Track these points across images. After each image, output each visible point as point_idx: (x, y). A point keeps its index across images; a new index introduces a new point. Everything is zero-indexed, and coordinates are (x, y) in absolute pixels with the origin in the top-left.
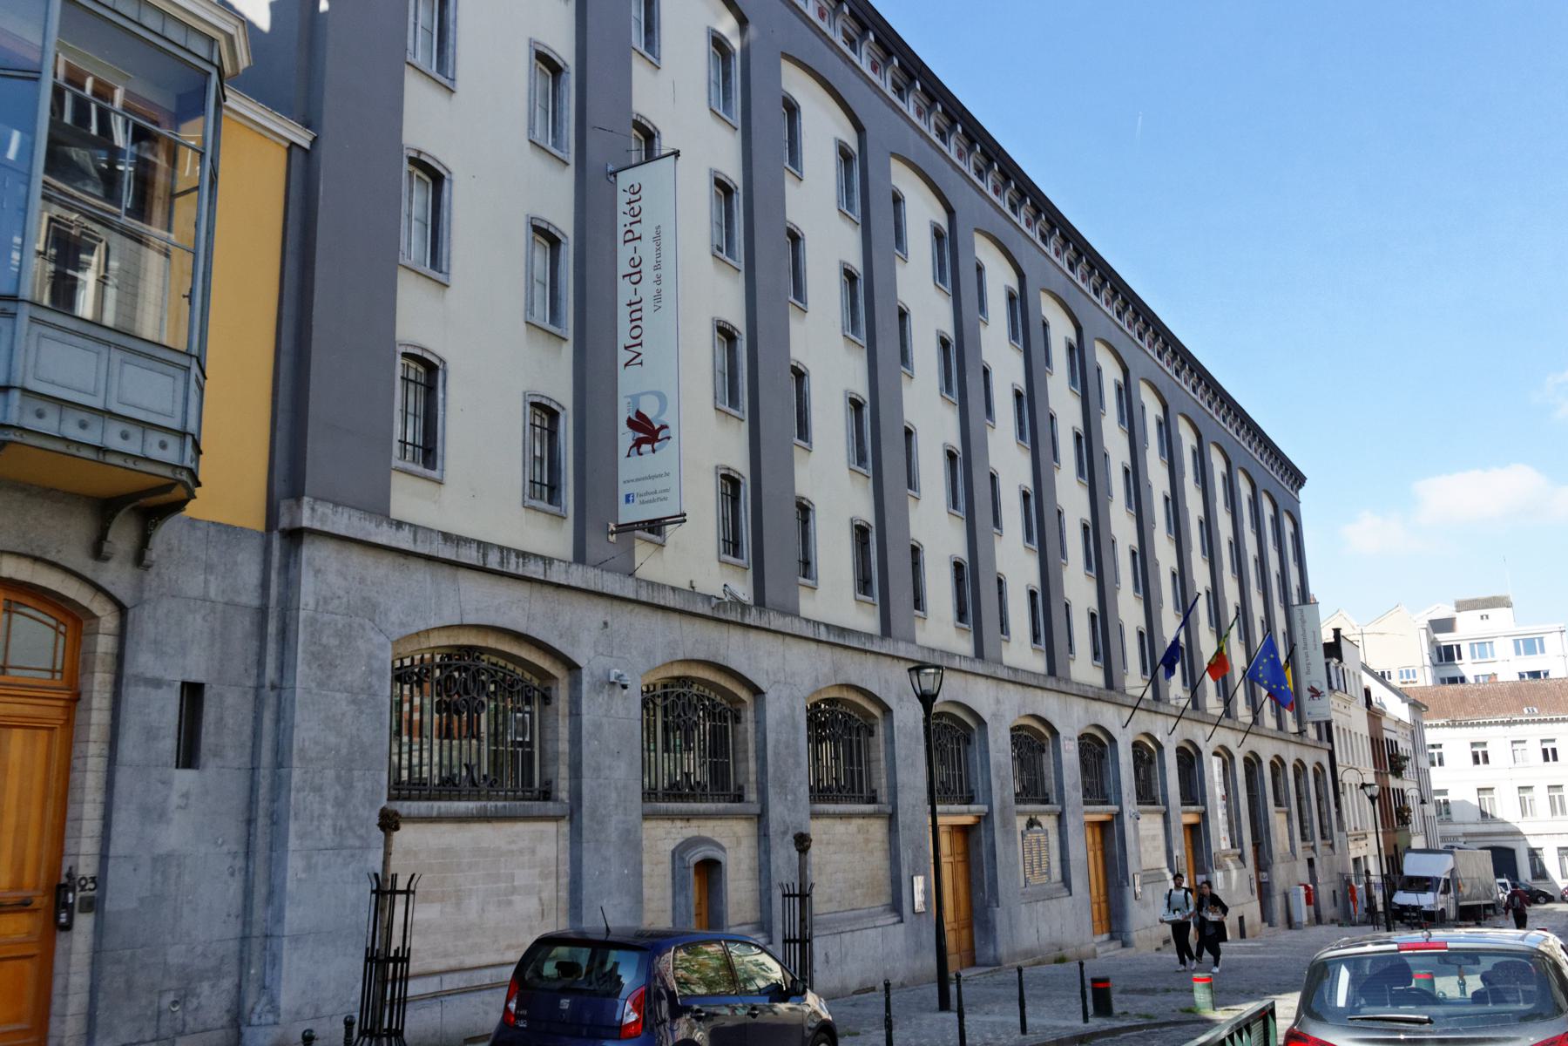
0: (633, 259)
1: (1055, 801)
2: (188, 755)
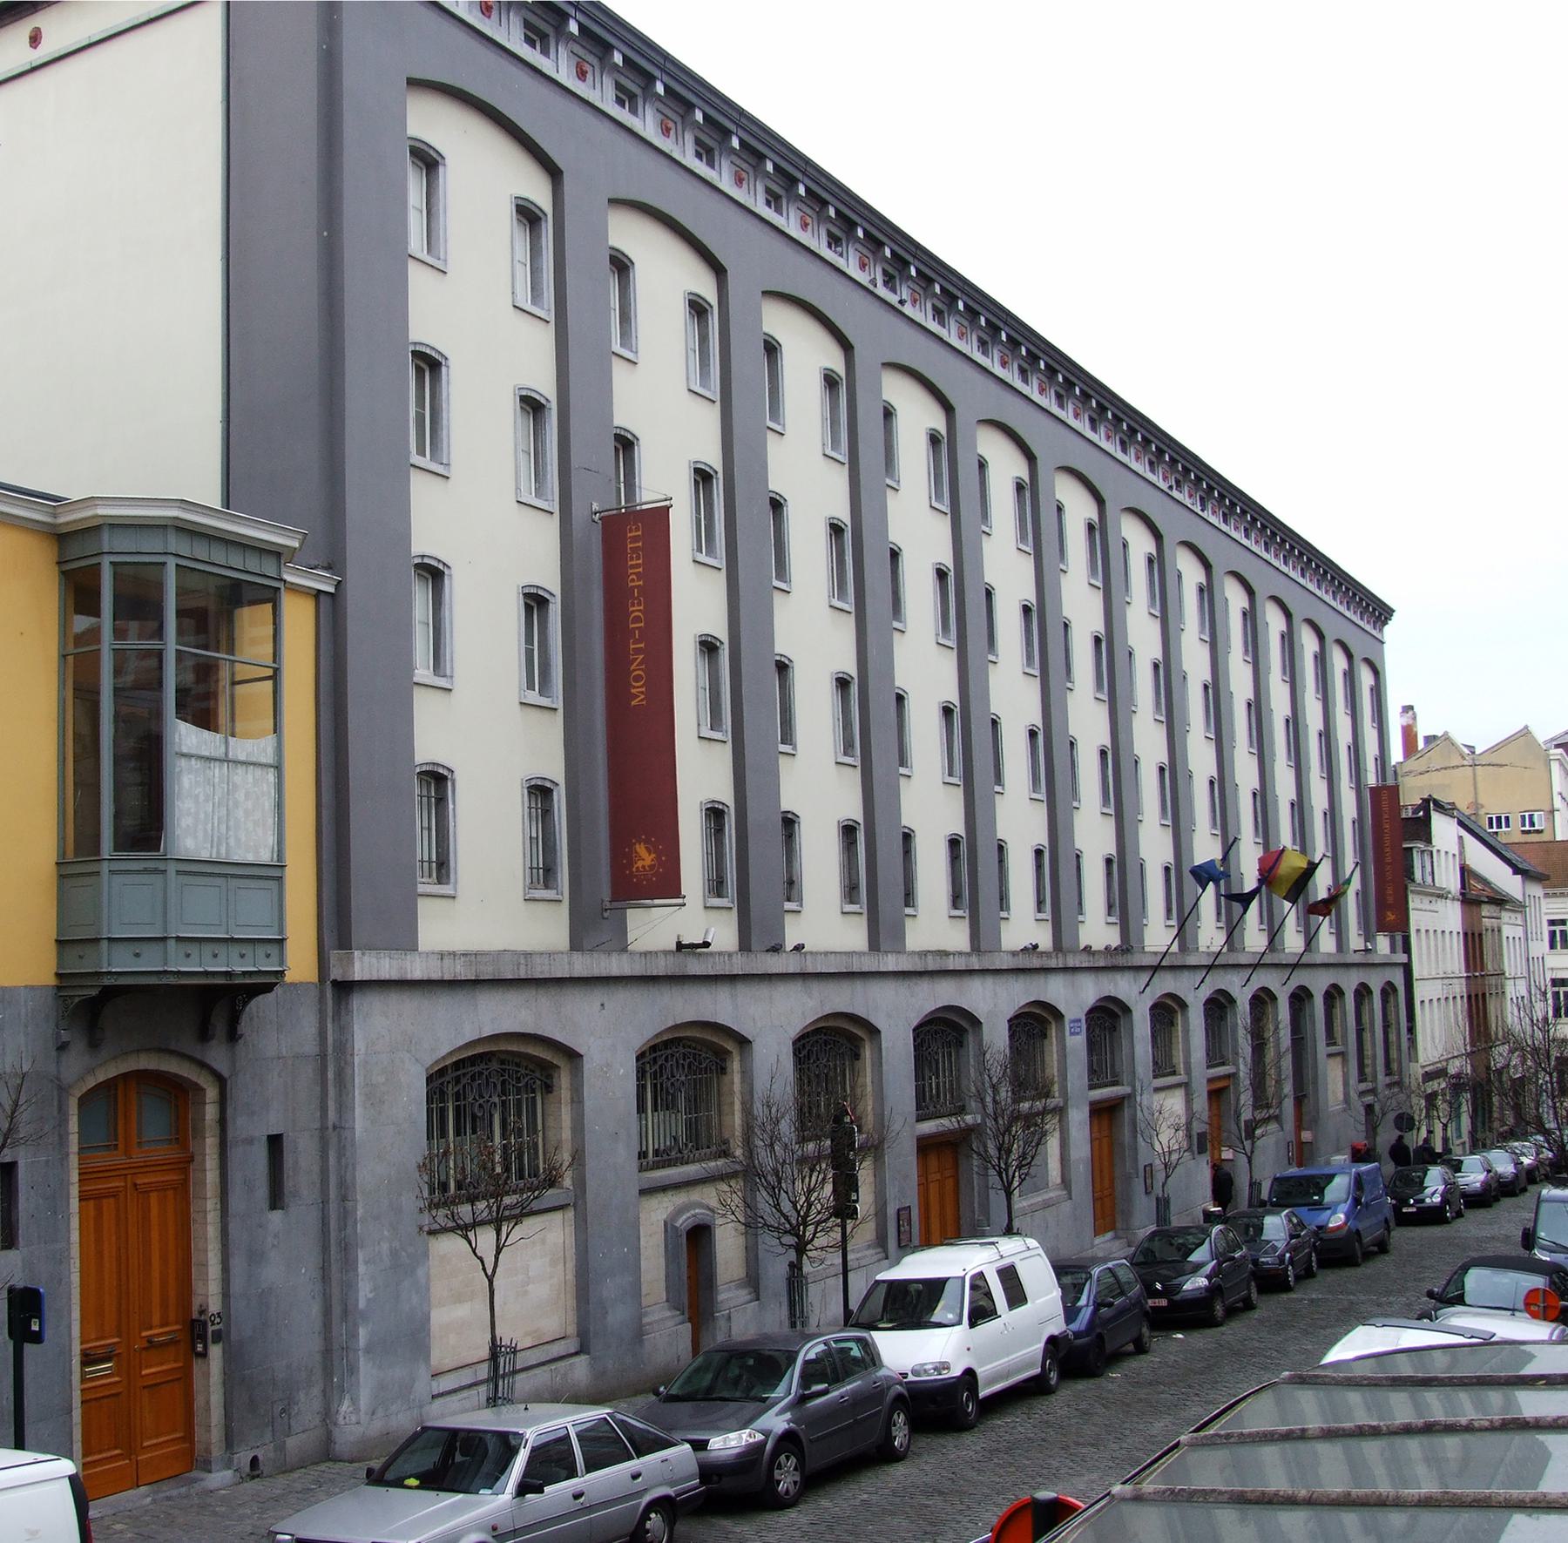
1: (1057, 1094)
2: (276, 1199)
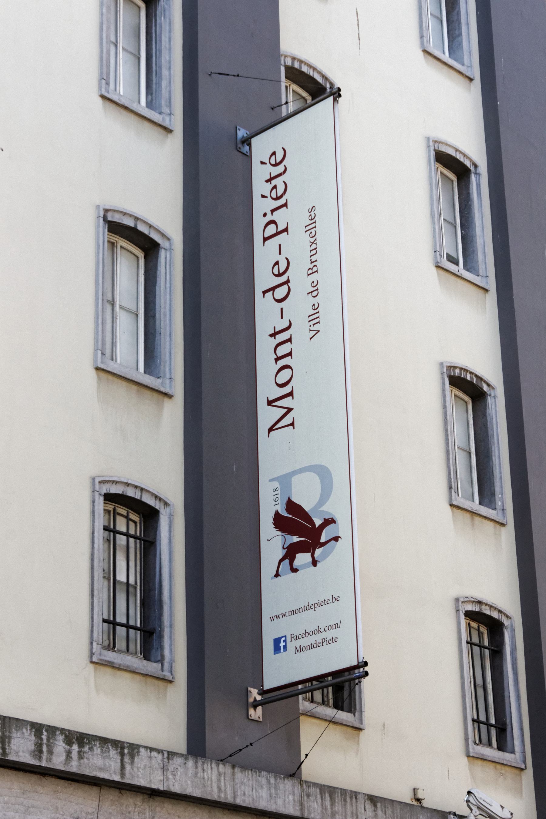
0: (277, 263)
